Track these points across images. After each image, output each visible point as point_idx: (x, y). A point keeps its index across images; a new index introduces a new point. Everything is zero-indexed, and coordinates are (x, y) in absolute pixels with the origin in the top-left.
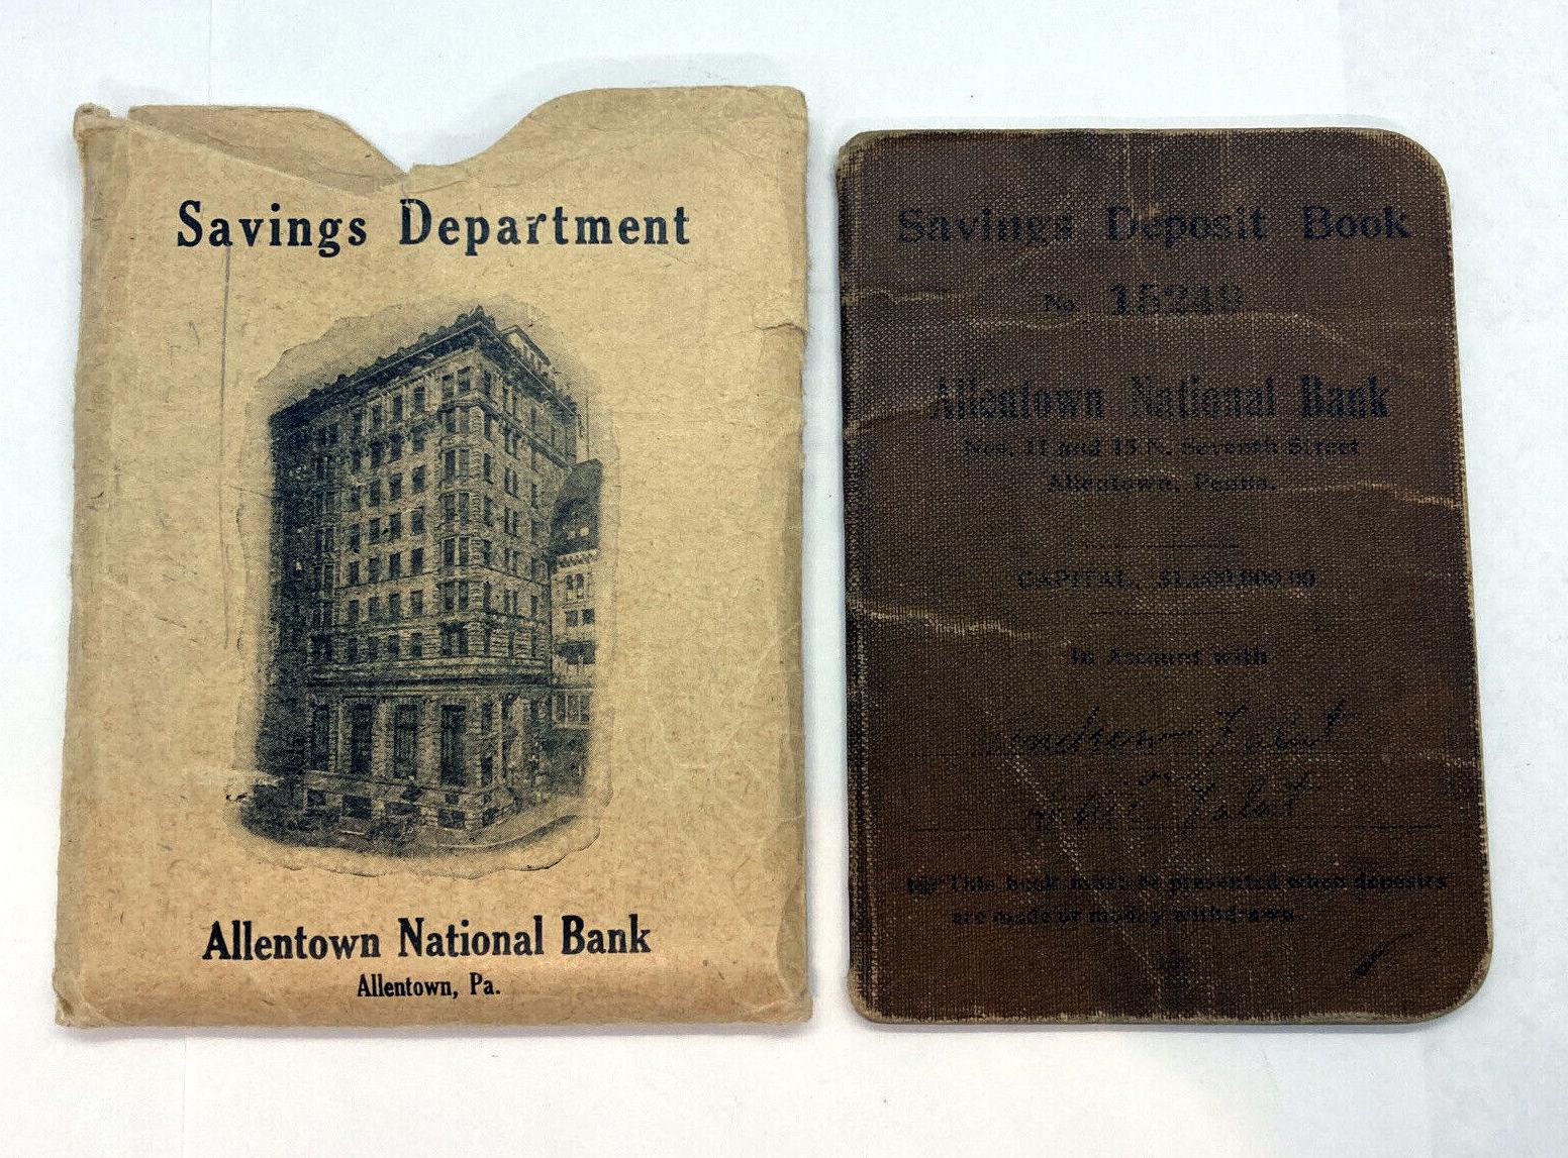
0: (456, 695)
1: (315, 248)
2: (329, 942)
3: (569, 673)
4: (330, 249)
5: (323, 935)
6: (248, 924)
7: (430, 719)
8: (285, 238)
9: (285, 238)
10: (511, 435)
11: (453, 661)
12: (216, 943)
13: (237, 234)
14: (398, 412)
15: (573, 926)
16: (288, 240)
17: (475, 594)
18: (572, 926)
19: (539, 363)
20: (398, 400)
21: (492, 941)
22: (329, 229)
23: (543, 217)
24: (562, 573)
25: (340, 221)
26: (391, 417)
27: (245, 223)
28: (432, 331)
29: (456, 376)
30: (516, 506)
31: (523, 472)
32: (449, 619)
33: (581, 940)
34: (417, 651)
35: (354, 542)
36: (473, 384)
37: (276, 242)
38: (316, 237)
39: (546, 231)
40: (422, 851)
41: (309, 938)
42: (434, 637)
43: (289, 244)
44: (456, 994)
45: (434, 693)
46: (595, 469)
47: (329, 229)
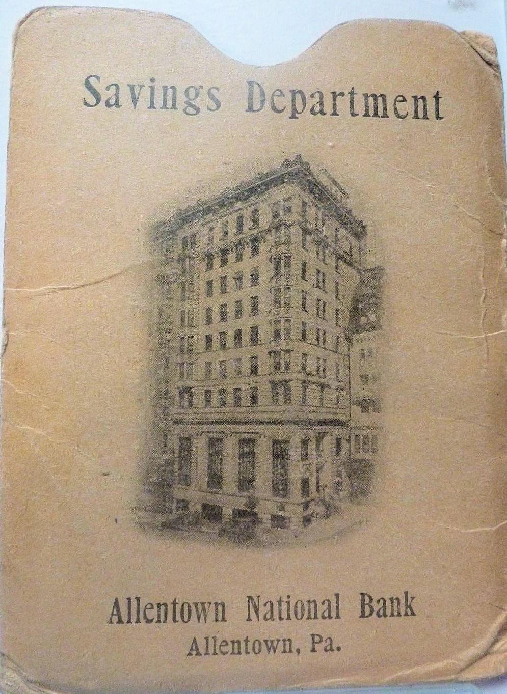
0: (281, 432)
1: (180, 111)
2: (263, 643)
3: (360, 418)
4: (193, 109)
5: (189, 602)
6: (138, 599)
7: (263, 450)
8: (159, 102)
9: (159, 102)
10: (321, 247)
11: (278, 409)
12: (115, 612)
13: (125, 98)
14: (240, 226)
15: (367, 600)
16: (117, 620)
17: (296, 360)
18: (366, 600)
19: (342, 197)
20: (240, 218)
21: (306, 607)
22: (192, 93)
23: (342, 94)
24: (356, 348)
25: (201, 87)
26: (235, 231)
27: (132, 87)
28: (265, 170)
29: (282, 202)
30: (324, 297)
31: (330, 271)
32: (277, 378)
33: (372, 609)
34: (254, 400)
35: (209, 320)
36: (293, 210)
37: (152, 106)
38: (181, 98)
39: (343, 104)
40: (259, 544)
41: (181, 604)
42: (265, 390)
43: (118, 622)
44: (298, 651)
45: (269, 430)
46: (376, 273)
47: (192, 93)
